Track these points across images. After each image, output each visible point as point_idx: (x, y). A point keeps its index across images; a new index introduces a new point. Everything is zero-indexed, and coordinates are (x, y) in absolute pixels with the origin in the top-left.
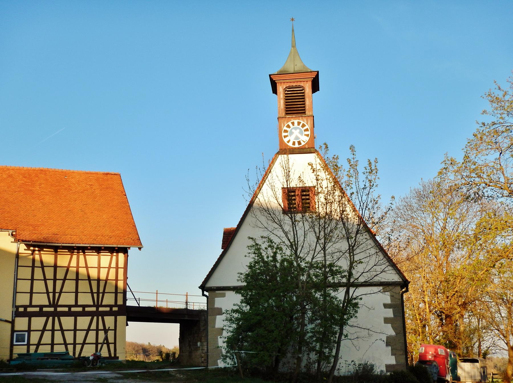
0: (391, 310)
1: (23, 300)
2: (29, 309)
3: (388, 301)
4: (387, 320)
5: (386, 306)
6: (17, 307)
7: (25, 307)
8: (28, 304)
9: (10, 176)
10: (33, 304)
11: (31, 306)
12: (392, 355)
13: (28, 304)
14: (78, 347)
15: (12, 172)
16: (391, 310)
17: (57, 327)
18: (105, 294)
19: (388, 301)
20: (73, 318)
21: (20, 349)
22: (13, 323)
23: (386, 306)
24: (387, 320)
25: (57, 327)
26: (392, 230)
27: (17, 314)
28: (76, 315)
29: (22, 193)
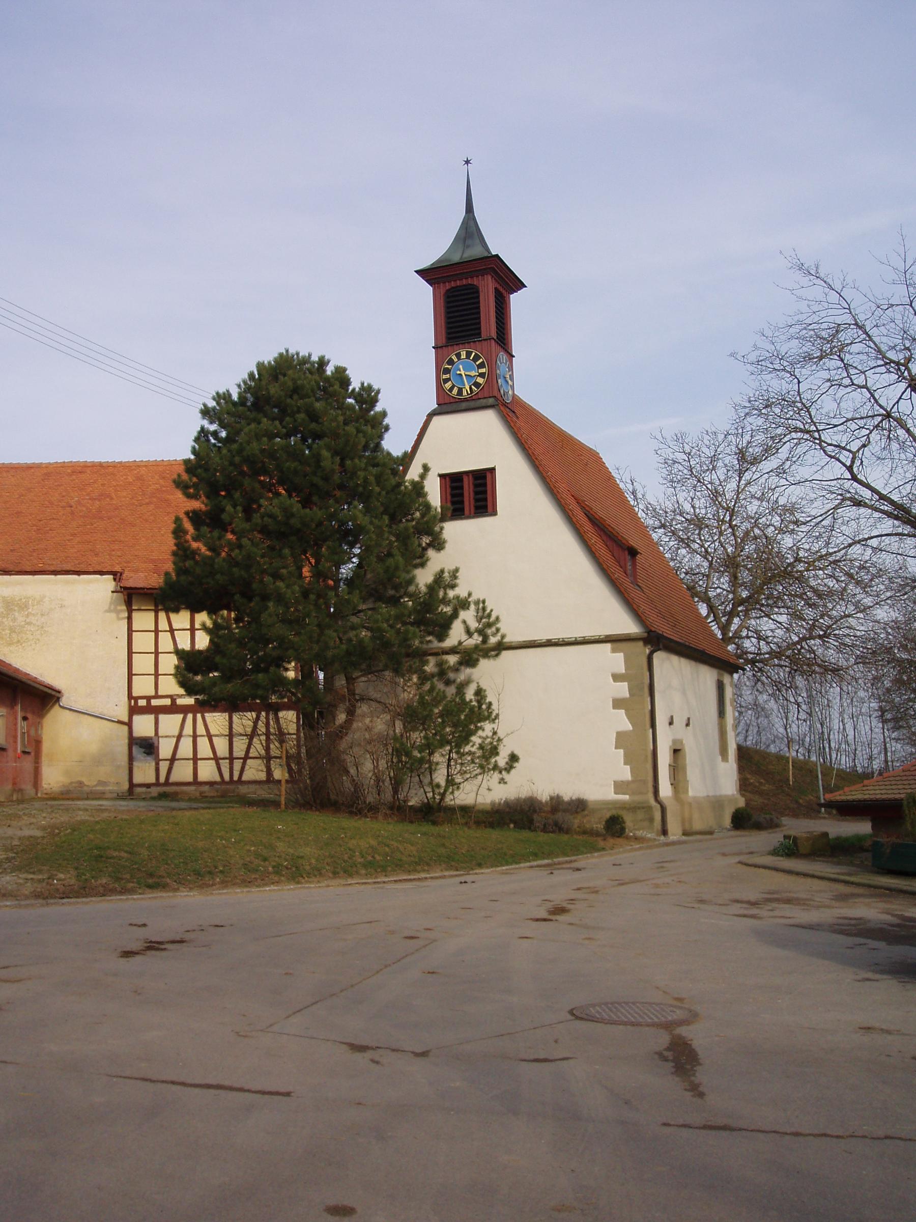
0: (625, 685)
1: (143, 687)
2: (154, 702)
3: (621, 669)
4: (618, 703)
5: (616, 677)
6: (136, 699)
7: (149, 699)
8: (153, 694)
9: (139, 478)
10: (160, 693)
11: (157, 696)
12: (625, 764)
13: (153, 694)
14: (237, 765)
15: (143, 471)
16: (625, 685)
17: (201, 730)
18: (160, 677)
19: (621, 669)
20: (152, 717)
21: (145, 772)
22: (129, 724)
23: (616, 677)
24: (618, 703)
25: (201, 730)
26: (42, 615)
27: (134, 710)
28: (157, 711)
29: (152, 507)
